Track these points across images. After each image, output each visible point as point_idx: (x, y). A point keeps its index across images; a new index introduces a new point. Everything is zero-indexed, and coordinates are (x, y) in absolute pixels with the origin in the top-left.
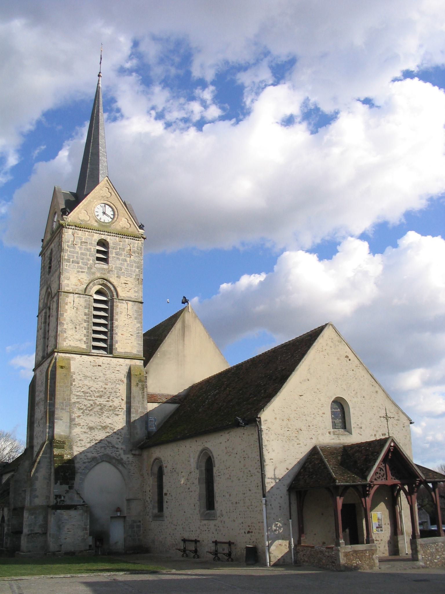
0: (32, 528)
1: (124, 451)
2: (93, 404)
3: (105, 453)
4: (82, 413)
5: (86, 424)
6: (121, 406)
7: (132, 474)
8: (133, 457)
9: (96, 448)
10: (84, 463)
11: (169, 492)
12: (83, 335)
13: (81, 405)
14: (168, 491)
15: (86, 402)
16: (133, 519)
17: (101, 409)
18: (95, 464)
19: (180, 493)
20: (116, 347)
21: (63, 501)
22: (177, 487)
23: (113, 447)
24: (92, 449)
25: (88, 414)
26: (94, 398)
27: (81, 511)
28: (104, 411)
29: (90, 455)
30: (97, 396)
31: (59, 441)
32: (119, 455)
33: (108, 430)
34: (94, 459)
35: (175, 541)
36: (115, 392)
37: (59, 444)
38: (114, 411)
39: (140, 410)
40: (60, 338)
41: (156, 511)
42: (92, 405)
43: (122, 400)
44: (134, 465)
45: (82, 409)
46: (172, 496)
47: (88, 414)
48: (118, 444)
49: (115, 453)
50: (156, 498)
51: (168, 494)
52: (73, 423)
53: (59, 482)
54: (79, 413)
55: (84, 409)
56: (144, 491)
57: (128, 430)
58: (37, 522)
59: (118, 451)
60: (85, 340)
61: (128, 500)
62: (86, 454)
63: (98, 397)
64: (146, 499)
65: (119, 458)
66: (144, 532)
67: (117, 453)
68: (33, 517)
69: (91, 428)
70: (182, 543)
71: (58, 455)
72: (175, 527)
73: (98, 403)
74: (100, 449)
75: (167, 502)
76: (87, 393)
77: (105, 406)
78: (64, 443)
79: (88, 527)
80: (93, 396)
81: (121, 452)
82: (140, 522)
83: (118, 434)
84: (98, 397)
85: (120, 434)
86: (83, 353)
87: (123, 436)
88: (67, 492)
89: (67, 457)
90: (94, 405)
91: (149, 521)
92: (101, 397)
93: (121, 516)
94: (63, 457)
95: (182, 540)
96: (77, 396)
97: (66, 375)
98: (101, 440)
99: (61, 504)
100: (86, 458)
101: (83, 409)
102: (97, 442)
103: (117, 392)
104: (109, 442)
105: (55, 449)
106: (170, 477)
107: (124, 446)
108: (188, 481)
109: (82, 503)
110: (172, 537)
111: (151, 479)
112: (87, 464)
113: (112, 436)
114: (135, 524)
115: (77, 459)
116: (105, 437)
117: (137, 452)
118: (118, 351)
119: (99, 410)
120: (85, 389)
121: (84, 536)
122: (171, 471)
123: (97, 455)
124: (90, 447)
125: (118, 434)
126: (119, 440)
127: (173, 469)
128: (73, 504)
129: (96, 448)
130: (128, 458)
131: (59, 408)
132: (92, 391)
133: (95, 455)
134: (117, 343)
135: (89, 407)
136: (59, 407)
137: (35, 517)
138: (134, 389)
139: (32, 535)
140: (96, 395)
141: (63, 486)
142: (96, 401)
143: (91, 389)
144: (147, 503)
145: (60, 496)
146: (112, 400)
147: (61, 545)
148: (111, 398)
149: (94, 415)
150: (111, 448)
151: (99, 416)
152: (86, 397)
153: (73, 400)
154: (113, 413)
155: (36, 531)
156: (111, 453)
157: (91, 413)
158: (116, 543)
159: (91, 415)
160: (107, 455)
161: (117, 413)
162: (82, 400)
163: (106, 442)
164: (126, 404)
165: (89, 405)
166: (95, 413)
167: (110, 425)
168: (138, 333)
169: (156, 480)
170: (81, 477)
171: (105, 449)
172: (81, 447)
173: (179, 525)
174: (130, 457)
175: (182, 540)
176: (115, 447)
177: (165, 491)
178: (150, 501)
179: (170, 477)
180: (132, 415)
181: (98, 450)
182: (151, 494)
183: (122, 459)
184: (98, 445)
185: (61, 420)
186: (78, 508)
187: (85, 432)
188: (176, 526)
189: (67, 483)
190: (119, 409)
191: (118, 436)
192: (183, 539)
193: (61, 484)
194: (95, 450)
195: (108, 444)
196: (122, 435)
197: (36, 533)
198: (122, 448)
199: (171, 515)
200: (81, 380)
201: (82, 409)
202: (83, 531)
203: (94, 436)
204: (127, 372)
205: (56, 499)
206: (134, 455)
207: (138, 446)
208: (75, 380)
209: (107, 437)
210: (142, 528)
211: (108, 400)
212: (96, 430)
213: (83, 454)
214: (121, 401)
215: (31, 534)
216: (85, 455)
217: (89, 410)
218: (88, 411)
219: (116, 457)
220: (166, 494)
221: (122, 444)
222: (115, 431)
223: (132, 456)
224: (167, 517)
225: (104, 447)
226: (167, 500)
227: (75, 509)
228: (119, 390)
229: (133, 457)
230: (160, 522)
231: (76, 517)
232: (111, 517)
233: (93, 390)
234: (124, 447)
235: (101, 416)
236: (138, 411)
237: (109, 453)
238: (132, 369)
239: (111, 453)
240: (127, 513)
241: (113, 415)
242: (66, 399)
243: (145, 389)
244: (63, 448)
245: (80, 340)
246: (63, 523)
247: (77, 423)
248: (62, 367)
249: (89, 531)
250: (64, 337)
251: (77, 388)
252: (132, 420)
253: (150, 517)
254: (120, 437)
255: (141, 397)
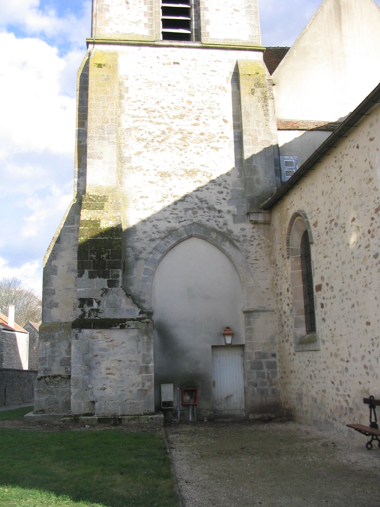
0: (47, 366)
1: (234, 215)
2: (167, 131)
3: (195, 220)
4: (145, 147)
5: (154, 167)
6: (223, 133)
7: (254, 262)
8: (254, 228)
9: (175, 212)
10: (152, 240)
11: (326, 281)
12: (142, 14)
13: (142, 132)
14: (322, 278)
15: (152, 128)
16: (261, 350)
17: (183, 139)
18: (174, 242)
19: (351, 276)
20: (207, 31)
21: (97, 310)
22: (343, 263)
23: (210, 208)
24: (167, 214)
25: (157, 149)
26: (167, 120)
27: (136, 332)
28: (189, 143)
29: (163, 226)
30: (173, 116)
31: (94, 196)
32: (225, 224)
33: (199, 176)
34: (171, 232)
35: (347, 401)
36: (209, 108)
37: (93, 201)
38: (210, 142)
39: (260, 138)
40: (98, 21)
41: (302, 331)
42: (163, 133)
43: (225, 121)
44: (256, 242)
45: (143, 140)
46: (332, 287)
47: (157, 149)
48: (221, 204)
49: (216, 221)
50: (301, 302)
51: (324, 288)
52: (128, 165)
53: (86, 271)
54: (140, 146)
55: (148, 140)
56: (278, 294)
57: (240, 177)
58: (56, 354)
59: (220, 217)
60: (146, 22)
61: (248, 313)
62: (155, 223)
63: (175, 117)
64: (282, 308)
65: (225, 230)
66: (282, 378)
67: (221, 220)
68: (48, 344)
69: (164, 175)
70: (366, 407)
71: (89, 220)
72: (345, 364)
73: (176, 129)
74: (183, 213)
75: (322, 306)
76: (154, 111)
77: (191, 133)
78: (104, 199)
79: (152, 365)
80: (165, 116)
81: (229, 218)
82: (274, 355)
83: (220, 185)
84: (175, 117)
85: (223, 183)
86: (142, 42)
87: (231, 188)
88: (106, 291)
89: (105, 225)
90: (169, 132)
91: (290, 354)
92: (182, 117)
93: (233, 344)
94: (99, 225)
95: (366, 401)
96: (133, 117)
97: (109, 78)
98: (186, 196)
99: (93, 318)
100: (155, 230)
101: (146, 139)
102: (177, 199)
103: (215, 109)
104: (201, 201)
105: (85, 210)
106: (325, 245)
107: (234, 206)
108: (373, 237)
109: (136, 314)
110: (338, 389)
111: (288, 262)
112: (158, 242)
113: (208, 189)
114: (264, 361)
115: (137, 232)
116: (194, 191)
117: (260, 218)
118: (211, 37)
119: (179, 142)
120: (151, 105)
121: (143, 384)
122: (326, 228)
123: (177, 226)
124: (164, 210)
125: (220, 185)
126: (223, 196)
127: (331, 221)
128: (118, 317)
129: (175, 212)
130: (243, 230)
131: (96, 137)
132: (163, 108)
133: (174, 224)
134: (208, 25)
135: (159, 136)
136: (94, 135)
137: (53, 345)
138: (246, 99)
139: (47, 379)
140: (171, 115)
141: (95, 280)
142: (172, 125)
143: (161, 104)
144: (284, 316)
145: (90, 302)
146: (204, 123)
147: (93, 402)
148: (202, 119)
149: (168, 150)
150: (206, 210)
151: (180, 152)
152: (152, 119)
153: (125, 126)
154: (208, 146)
155: (55, 373)
156: (208, 221)
157: (163, 146)
158: (228, 398)
159: (163, 150)
160: (199, 225)
161: (215, 145)
162: (144, 123)
163: (197, 201)
164: (234, 129)
165: (159, 133)
166: (170, 147)
167: (202, 169)
168: (248, 7)
169: (299, 264)
170: (145, 267)
171: (195, 213)
172: (144, 209)
173: (355, 360)
174: (248, 226)
175: (366, 401)
176: (215, 209)
177: (316, 281)
178: (290, 311)
179: (325, 245)
180: (245, 147)
181: (180, 214)
182: (291, 296)
183: (230, 232)
184: (180, 207)
185: (99, 158)
186: (129, 326)
187: (151, 182)
188: (347, 361)
189: (104, 275)
190: (220, 137)
191: (221, 189)
192: (368, 397)
193: (91, 276)
194: (173, 215)
195: (199, 204)
196: (227, 186)
197: (55, 377)
198: (229, 212)
199: (333, 337)
200: (140, 89)
201: (143, 140)
202: (140, 373)
203: (170, 189)
204: (230, 72)
205: (81, 306)
206: (255, 223)
207: (262, 205)
208: (129, 90)
209: (198, 190)
210: (278, 369)
211: (197, 122)
212: (173, 177)
213: (148, 223)
214: (223, 123)
215: (45, 377)
216: (154, 226)
217: (158, 142)
218: (156, 144)
219: (217, 227)
220: (319, 288)
221: (230, 202)
222: (213, 178)
223: (251, 226)
224: (323, 342)
225: (192, 209)
226: (324, 302)
227: (122, 327)
228: (218, 104)
229: (254, 228)
230: (311, 353)
231: (124, 345)
232: (213, 347)
233: (165, 107)
234: (233, 209)
235: (183, 152)
236: (256, 138)
237: (204, 221)
238: (238, 61)
239: (208, 221)
240: (246, 339)
241: (209, 149)
242: (110, 121)
243: (270, 102)
244: (102, 208)
245: (135, 23)
246: (96, 356)
247: (134, 166)
248: (100, 66)
249: (153, 374)
250: (106, 19)
251: (134, 104)
252: (247, 155)
253: (291, 345)
254: (225, 191)
255: (262, 113)
